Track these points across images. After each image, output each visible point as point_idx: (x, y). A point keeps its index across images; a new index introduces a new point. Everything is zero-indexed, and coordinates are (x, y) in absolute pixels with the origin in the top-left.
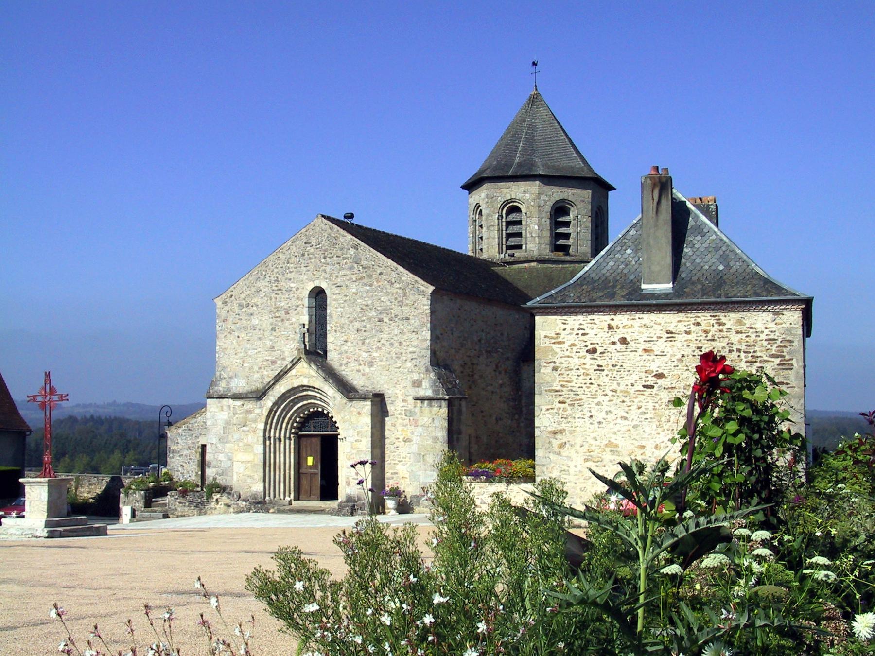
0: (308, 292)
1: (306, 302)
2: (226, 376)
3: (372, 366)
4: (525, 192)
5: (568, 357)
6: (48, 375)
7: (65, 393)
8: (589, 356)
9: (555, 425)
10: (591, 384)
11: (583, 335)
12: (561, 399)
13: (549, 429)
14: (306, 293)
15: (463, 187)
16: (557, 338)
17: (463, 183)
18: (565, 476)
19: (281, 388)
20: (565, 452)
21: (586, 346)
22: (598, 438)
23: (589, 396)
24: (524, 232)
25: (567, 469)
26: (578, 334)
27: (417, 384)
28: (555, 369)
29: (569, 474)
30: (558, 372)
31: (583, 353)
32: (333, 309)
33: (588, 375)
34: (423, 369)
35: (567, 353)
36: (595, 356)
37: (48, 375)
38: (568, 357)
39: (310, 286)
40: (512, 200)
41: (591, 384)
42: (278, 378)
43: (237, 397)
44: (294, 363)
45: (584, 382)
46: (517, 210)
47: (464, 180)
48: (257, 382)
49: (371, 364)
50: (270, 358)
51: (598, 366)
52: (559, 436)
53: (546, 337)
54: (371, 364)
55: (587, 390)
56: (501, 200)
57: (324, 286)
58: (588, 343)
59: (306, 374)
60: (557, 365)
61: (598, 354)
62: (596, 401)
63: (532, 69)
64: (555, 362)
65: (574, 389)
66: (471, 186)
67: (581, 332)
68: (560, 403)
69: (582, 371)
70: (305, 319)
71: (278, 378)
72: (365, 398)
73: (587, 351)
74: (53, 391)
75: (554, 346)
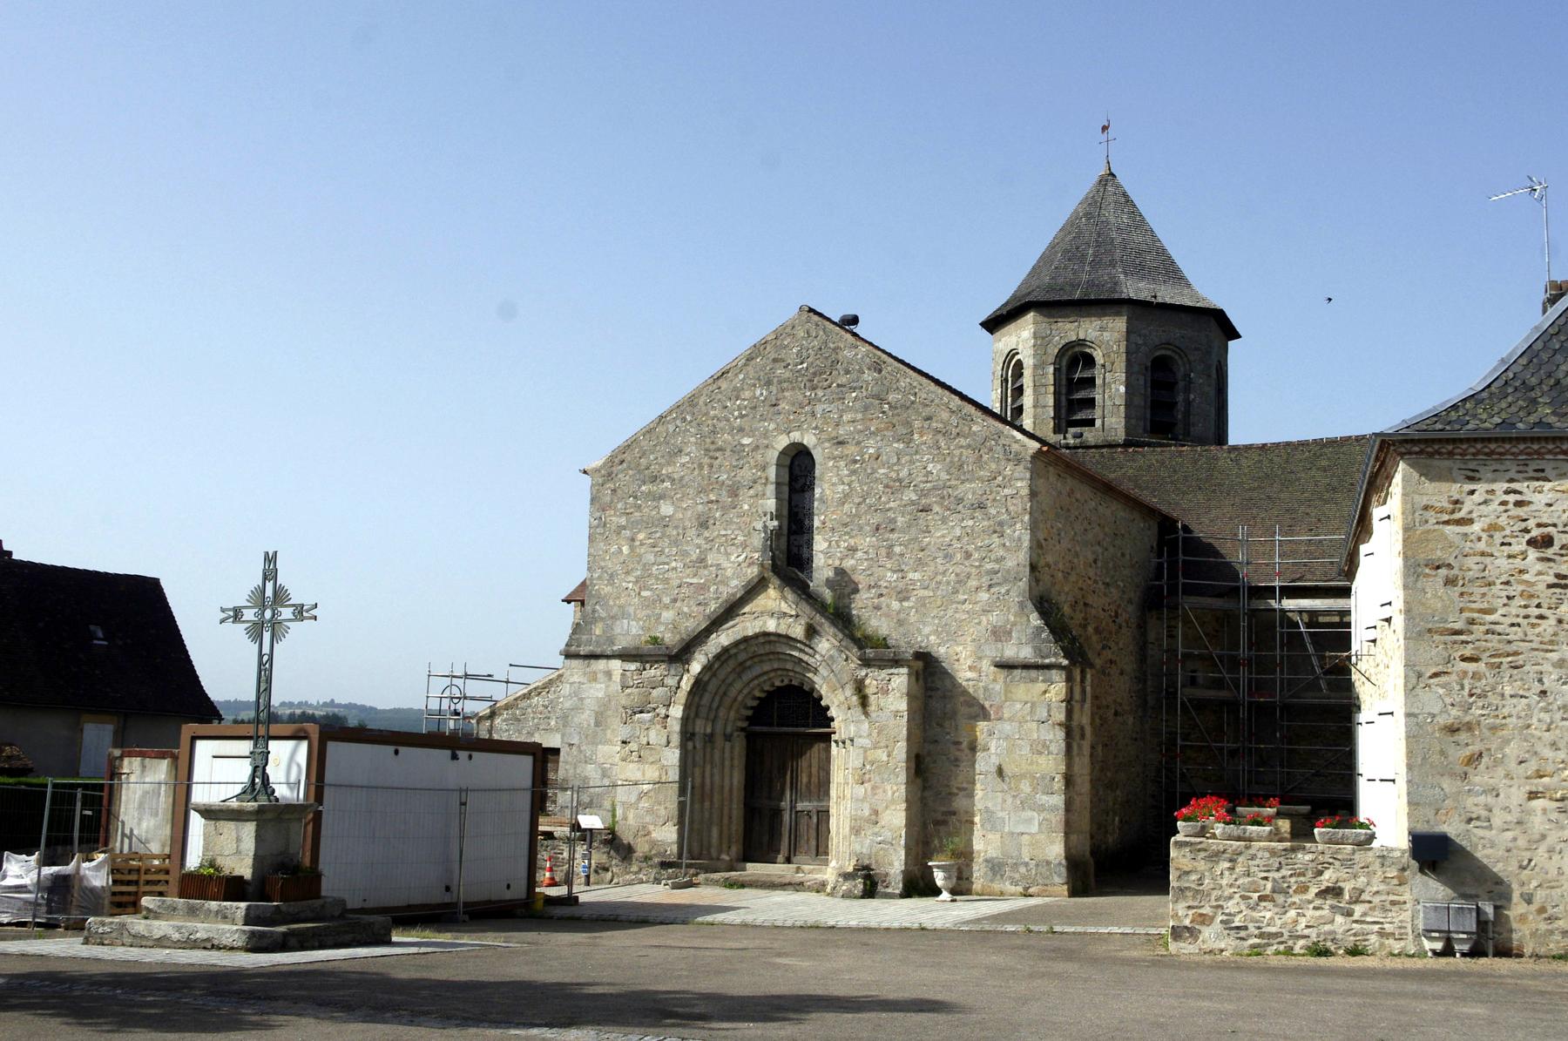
0: (776, 454)
1: (772, 472)
2: (603, 614)
3: (907, 599)
4: (1102, 329)
5: (1482, 554)
6: (271, 559)
7: (308, 602)
8: (1533, 554)
9: (1454, 712)
10: (1541, 617)
11: (1518, 504)
12: (1468, 652)
13: (1442, 720)
14: (773, 456)
15: (984, 325)
16: (1453, 512)
17: (983, 318)
18: (1480, 832)
19: (723, 638)
20: (1480, 778)
21: (1527, 531)
22: (1562, 744)
23: (1534, 645)
24: (1098, 398)
25: (1484, 813)
26: (1504, 503)
27: (999, 634)
28: (1450, 582)
29: (1490, 828)
30: (1458, 589)
31: (1519, 545)
32: (828, 486)
33: (1532, 596)
34: (1015, 608)
35: (1481, 546)
36: (1549, 552)
37: (271, 559)
38: (1482, 554)
39: (782, 442)
40: (1081, 343)
41: (1541, 617)
42: (717, 623)
43: (625, 656)
44: (754, 590)
45: (1523, 612)
46: (1089, 361)
47: (987, 312)
48: (670, 626)
49: (903, 596)
50: (695, 581)
51: (1558, 576)
52: (1463, 737)
53: (1426, 508)
54: (903, 596)
55: (1530, 631)
56: (1058, 342)
57: (809, 440)
58: (1531, 524)
59: (774, 612)
60: (1455, 571)
61: (1556, 548)
62: (1554, 656)
63: (1103, 137)
64: (1449, 566)
65: (1498, 628)
66: (994, 324)
67: (1512, 498)
68: (1464, 659)
69: (1515, 589)
70: (771, 504)
71: (717, 623)
72: (896, 662)
73: (1529, 543)
74: (280, 596)
75: (1449, 529)
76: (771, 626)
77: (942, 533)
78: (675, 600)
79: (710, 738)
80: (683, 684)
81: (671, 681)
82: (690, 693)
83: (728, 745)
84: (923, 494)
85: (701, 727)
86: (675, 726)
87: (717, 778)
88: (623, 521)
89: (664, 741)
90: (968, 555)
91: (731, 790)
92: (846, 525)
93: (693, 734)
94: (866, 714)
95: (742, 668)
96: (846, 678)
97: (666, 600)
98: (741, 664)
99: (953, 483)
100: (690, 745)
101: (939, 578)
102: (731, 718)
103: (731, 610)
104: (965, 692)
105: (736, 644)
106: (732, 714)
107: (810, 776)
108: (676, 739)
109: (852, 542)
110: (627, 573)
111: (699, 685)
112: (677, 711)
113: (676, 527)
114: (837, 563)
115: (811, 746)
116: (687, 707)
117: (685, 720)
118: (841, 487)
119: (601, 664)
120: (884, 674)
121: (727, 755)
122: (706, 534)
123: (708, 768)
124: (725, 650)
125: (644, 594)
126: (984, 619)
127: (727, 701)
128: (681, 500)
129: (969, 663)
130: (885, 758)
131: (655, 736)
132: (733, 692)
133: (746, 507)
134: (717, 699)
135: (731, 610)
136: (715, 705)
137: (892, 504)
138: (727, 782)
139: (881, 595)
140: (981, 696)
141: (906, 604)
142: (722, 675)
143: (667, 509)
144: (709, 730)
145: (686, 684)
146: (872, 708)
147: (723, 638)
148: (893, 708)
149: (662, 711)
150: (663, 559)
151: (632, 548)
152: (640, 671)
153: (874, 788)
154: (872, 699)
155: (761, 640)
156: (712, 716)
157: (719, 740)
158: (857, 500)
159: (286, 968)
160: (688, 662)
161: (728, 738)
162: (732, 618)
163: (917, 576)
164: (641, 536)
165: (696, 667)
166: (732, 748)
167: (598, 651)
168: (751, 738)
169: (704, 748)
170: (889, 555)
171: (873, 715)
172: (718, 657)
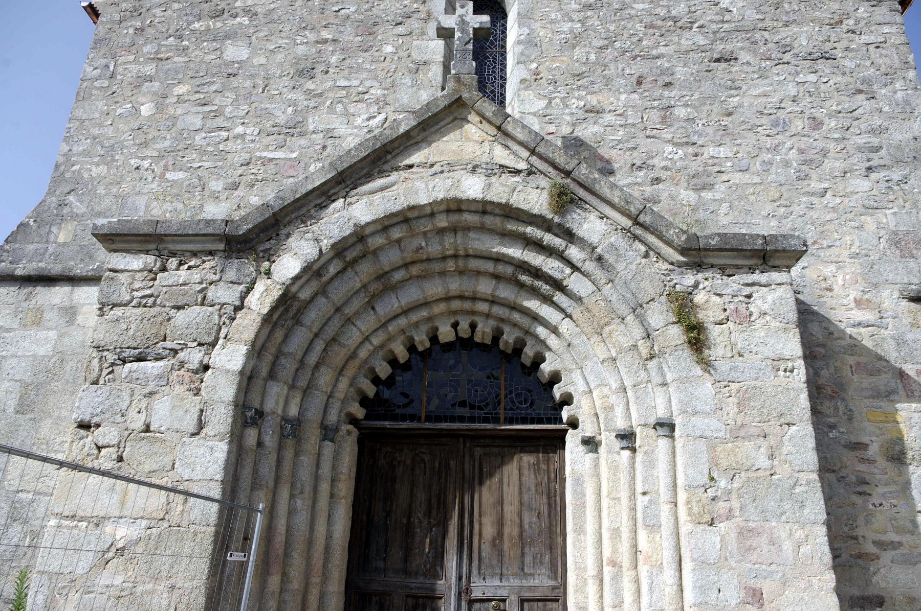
19: (362, 208)
42: (347, 179)
50: (280, 154)
71: (347, 179)
76: (473, 188)
77: (753, 95)
78: (235, 186)
79: (292, 429)
80: (253, 300)
81: (225, 294)
82: (267, 319)
83: (328, 448)
84: (717, 36)
85: (275, 399)
86: (222, 389)
87: (302, 519)
88: (150, 69)
89: (190, 423)
90: (816, 124)
91: (327, 549)
92: (579, 76)
93: (260, 414)
94: (706, 365)
95: (385, 284)
96: (649, 289)
97: (216, 185)
98: (382, 276)
99: (768, 23)
100: (251, 436)
101: (767, 156)
102: (338, 393)
103: (381, 158)
104: (855, 347)
105: (386, 224)
106: (344, 384)
107: (500, 523)
108: (221, 418)
109: (593, 100)
110: (145, 144)
111: (287, 309)
112: (231, 357)
113: (252, 77)
114: (566, 130)
115: (504, 460)
116: (257, 350)
117: (248, 380)
118: (566, 26)
119: (59, 294)
120: (735, 283)
121: (326, 470)
122: (310, 85)
123: (284, 493)
124: (360, 235)
125: (170, 176)
126: (869, 221)
127: (339, 355)
128: (267, 38)
129: (853, 294)
130: (763, 462)
131: (170, 410)
132: (353, 336)
133: (389, 49)
134: (319, 346)
135: (381, 158)
136: (312, 359)
137: (662, 50)
138: (321, 528)
139: (657, 180)
140: (892, 354)
141: (707, 195)
142: (338, 292)
143: (235, 52)
144: (293, 411)
145: (262, 299)
146: (717, 352)
147: (362, 208)
148: (767, 352)
149: (194, 356)
150: (220, 122)
151: (160, 107)
152: (152, 274)
153: (744, 533)
154: (715, 332)
155: (442, 222)
156: (302, 383)
157: (312, 435)
158: (599, 43)
159: (354, 470)
160: (270, 256)
161: (328, 433)
162: (382, 173)
163: (723, 152)
164: (181, 89)
165: (288, 265)
166: (336, 457)
167: (57, 269)
168: (370, 444)
169: (280, 448)
170: (666, 121)
171: (723, 367)
172: (340, 249)
